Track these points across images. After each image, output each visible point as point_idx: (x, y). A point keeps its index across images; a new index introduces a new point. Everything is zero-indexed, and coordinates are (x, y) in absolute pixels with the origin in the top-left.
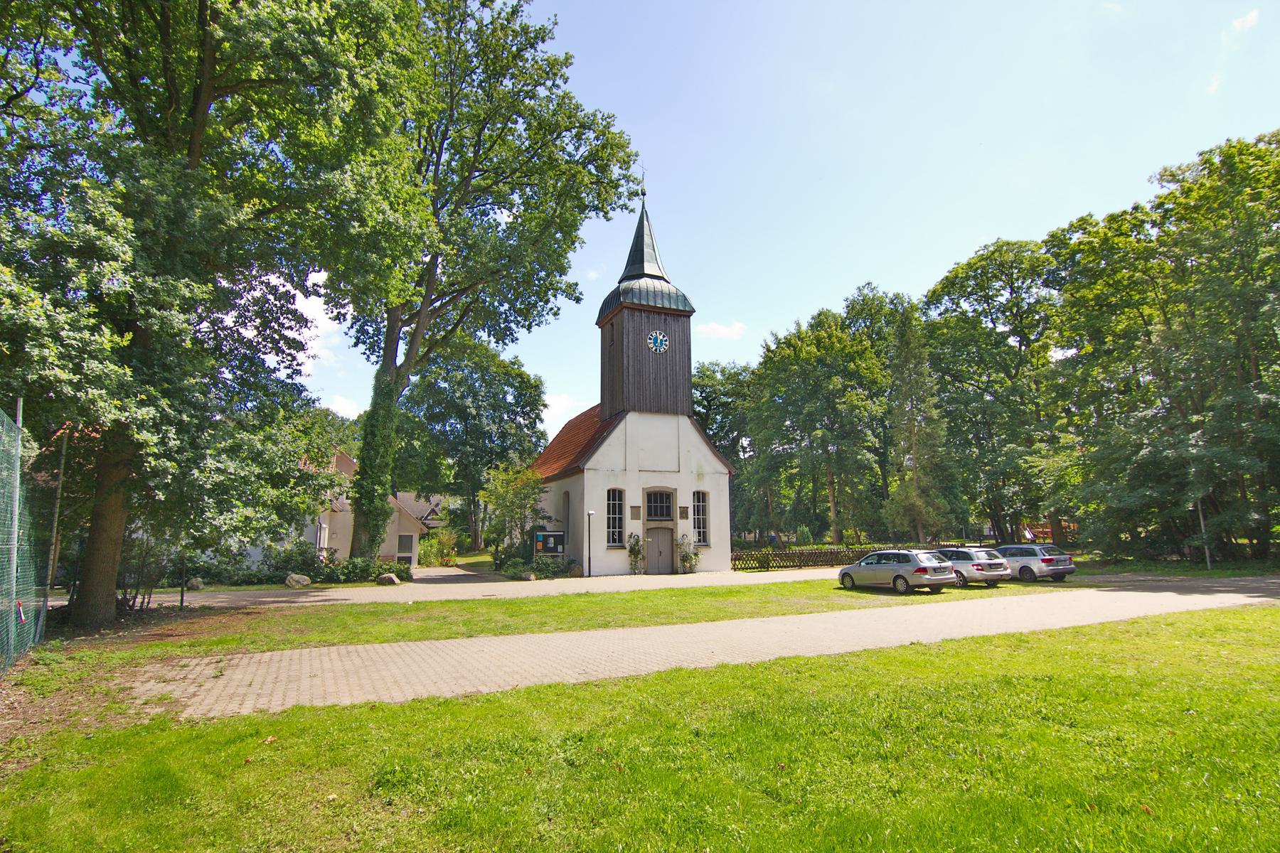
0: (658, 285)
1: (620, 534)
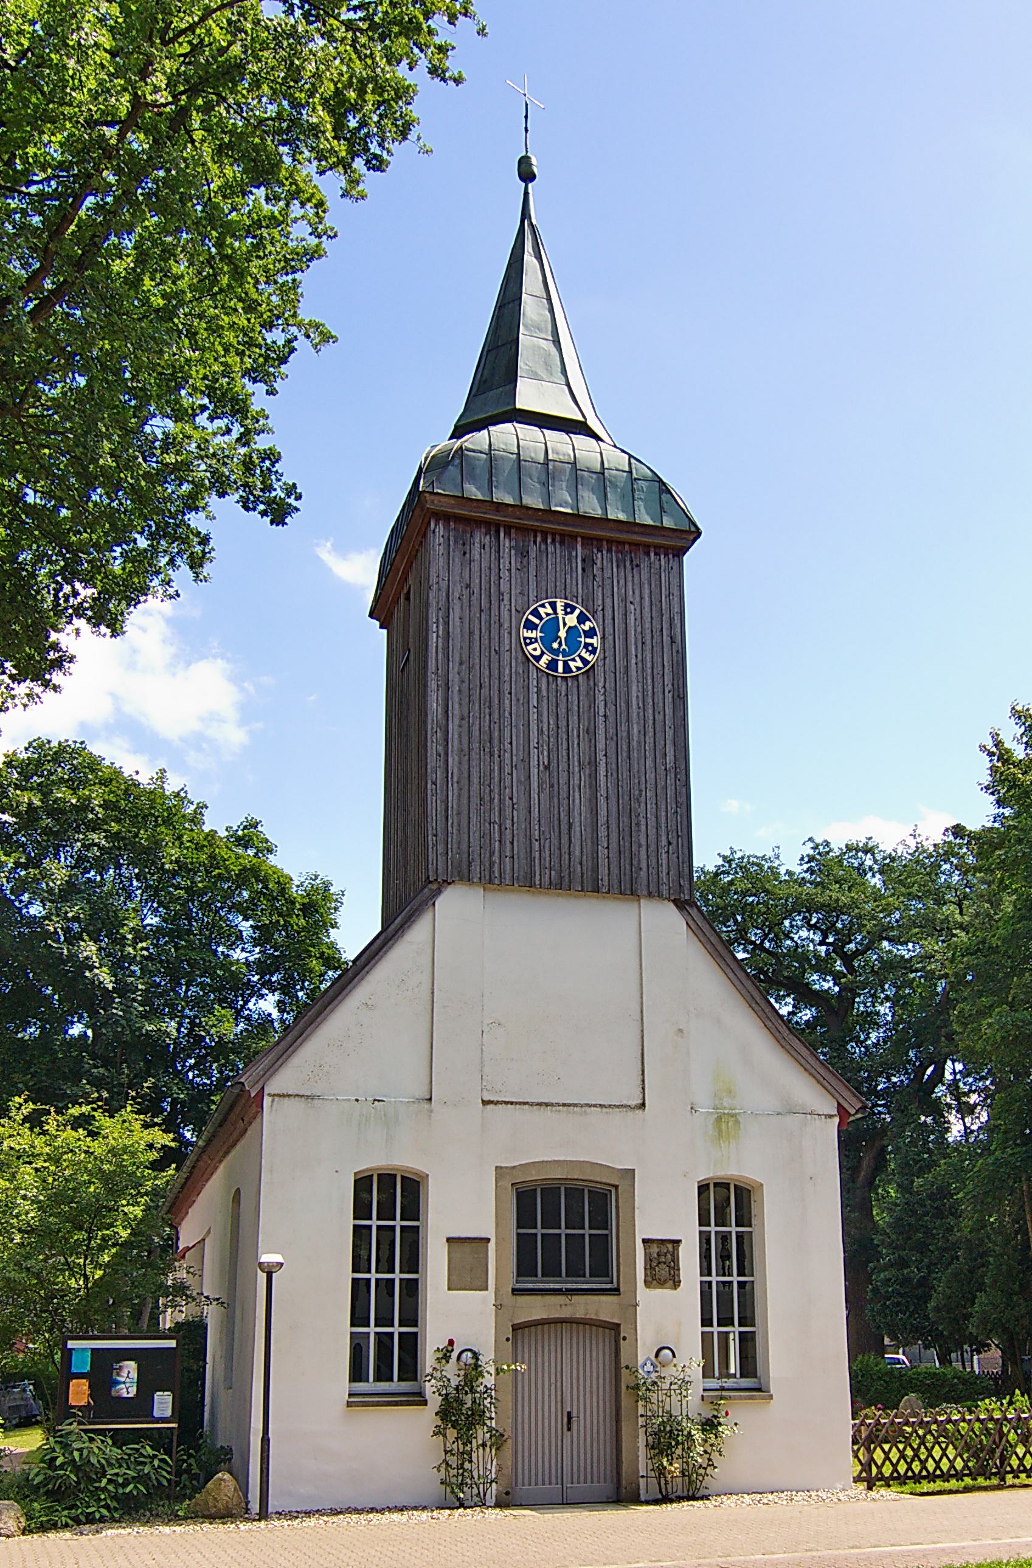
0: (559, 443)
1: (411, 1344)
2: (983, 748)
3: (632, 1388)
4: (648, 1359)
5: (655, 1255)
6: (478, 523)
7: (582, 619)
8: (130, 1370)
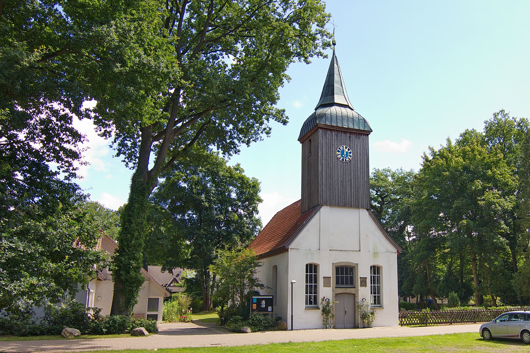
1: (315, 297)
2: (422, 157)
6: (328, 129)
7: (349, 150)
8: (264, 302)
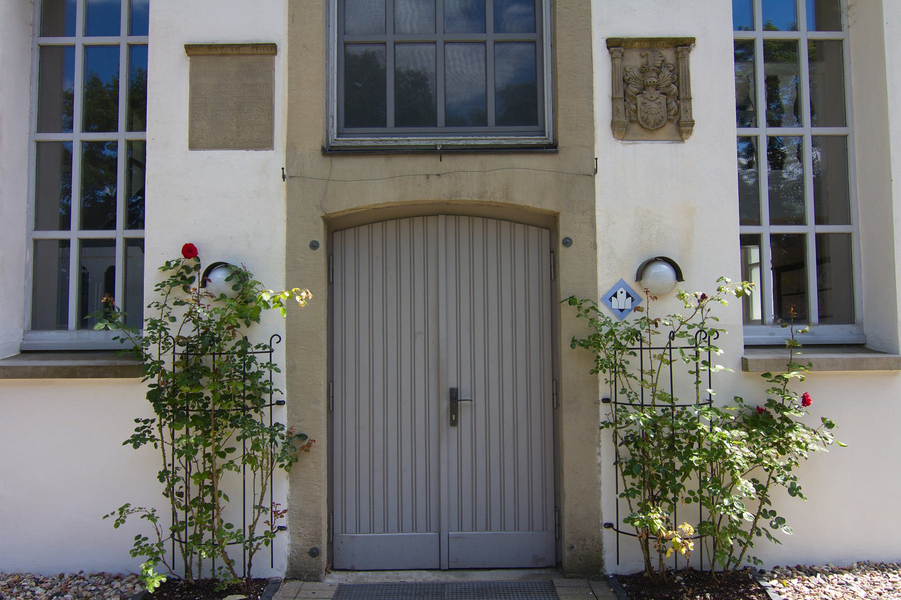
3: (585, 344)
4: (621, 283)
5: (636, 73)
